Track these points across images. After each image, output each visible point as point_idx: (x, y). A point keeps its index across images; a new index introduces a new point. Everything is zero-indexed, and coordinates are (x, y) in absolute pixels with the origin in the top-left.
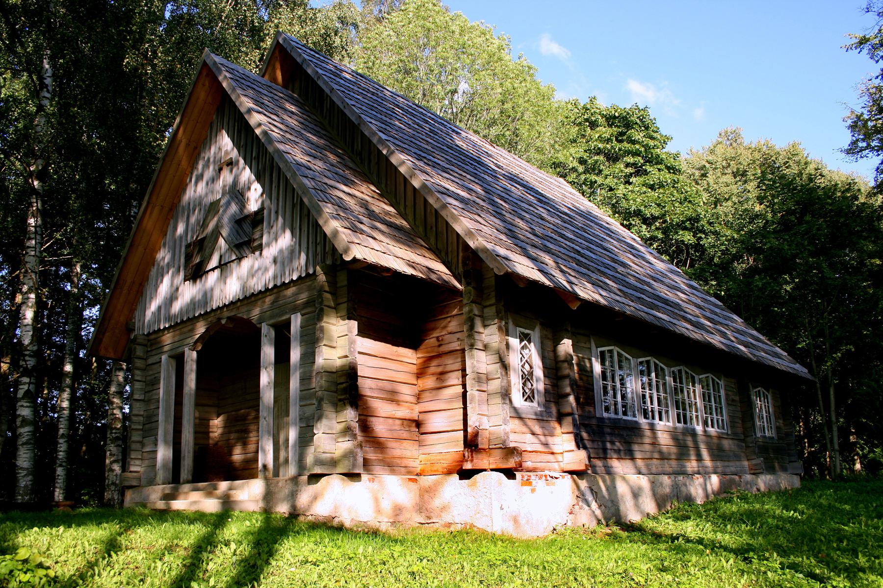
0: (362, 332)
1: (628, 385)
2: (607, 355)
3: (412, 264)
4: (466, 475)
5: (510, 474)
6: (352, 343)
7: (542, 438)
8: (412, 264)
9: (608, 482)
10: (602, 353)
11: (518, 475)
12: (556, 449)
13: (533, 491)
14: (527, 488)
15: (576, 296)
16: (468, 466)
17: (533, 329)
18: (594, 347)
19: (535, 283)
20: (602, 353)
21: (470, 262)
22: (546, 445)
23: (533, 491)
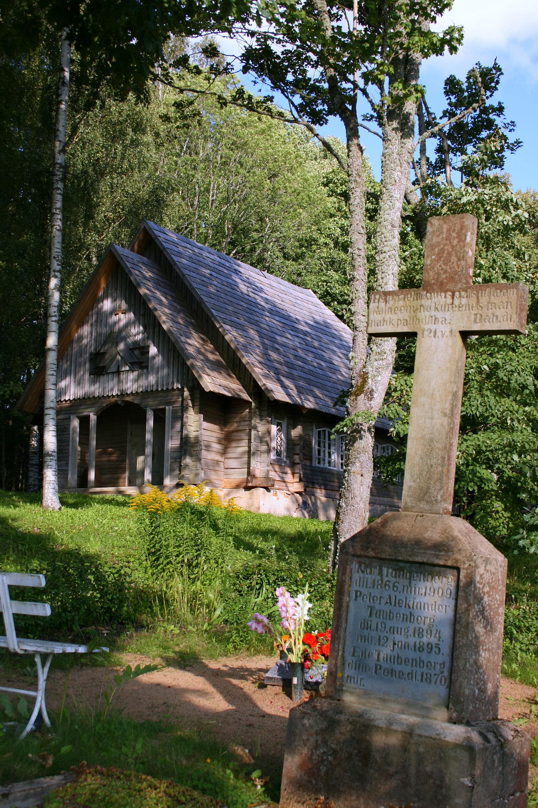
0: (205, 420)
1: (333, 457)
2: (322, 434)
3: (225, 388)
4: (248, 488)
5: (267, 489)
6: (201, 424)
7: (280, 474)
8: (225, 388)
9: (313, 500)
10: (319, 432)
11: (272, 491)
12: (287, 480)
13: (278, 499)
14: (275, 498)
15: (303, 407)
16: (250, 485)
17: (283, 420)
18: (381, 728)
19: (287, 403)
20: (384, 448)
21: (259, 393)
22: (282, 478)
23: (278, 499)
